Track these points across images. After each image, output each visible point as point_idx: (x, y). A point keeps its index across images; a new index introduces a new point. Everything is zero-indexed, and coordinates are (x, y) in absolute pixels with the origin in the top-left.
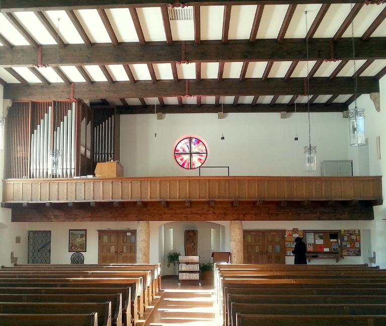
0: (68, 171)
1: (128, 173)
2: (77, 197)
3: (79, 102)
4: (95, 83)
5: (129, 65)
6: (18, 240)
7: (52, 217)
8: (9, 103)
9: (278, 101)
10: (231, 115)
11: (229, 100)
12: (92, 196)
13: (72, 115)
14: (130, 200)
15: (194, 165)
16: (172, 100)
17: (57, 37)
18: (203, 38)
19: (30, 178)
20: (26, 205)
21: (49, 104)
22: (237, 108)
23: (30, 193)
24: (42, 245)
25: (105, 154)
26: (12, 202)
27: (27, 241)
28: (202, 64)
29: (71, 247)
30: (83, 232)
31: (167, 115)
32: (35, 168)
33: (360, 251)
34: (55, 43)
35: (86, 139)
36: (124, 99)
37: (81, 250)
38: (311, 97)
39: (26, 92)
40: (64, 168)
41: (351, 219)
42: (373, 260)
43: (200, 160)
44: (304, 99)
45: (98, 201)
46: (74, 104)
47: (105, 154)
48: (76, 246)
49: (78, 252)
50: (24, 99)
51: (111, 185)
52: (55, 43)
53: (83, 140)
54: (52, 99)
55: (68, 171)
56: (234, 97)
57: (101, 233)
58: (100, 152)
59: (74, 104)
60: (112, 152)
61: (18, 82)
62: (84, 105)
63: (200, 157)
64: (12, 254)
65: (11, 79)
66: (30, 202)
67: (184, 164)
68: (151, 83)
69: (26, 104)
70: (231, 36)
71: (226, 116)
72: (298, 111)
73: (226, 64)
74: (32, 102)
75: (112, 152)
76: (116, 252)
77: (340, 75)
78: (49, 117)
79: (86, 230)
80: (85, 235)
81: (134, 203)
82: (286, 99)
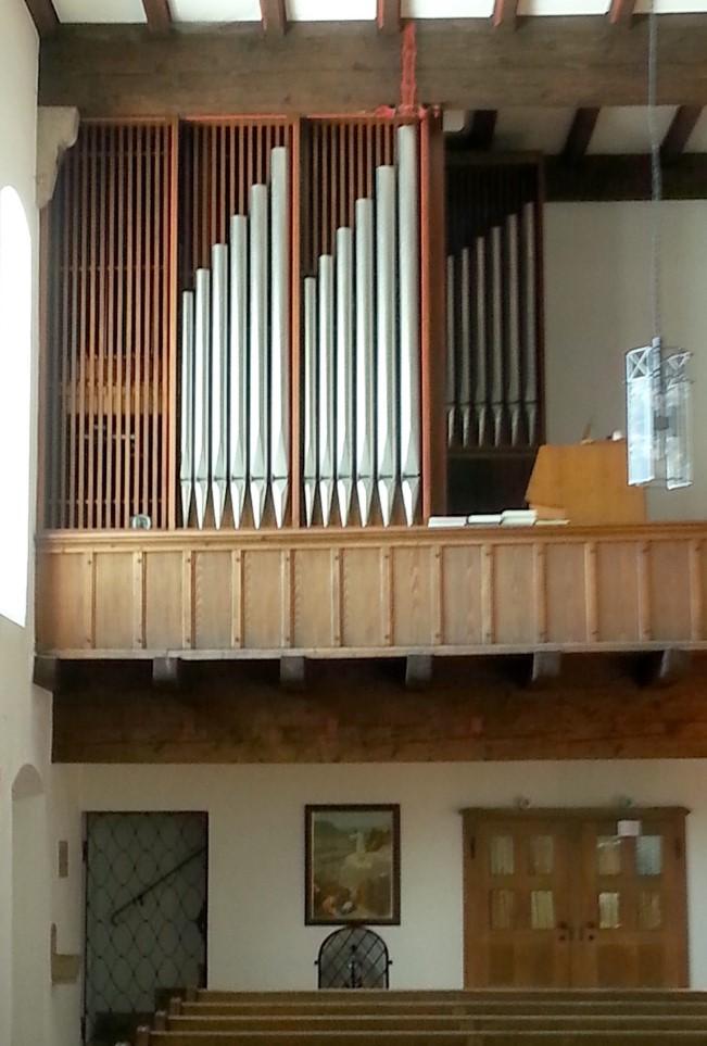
0: (257, 490)
2: (451, 631)
8: (66, 126)
14: (234, 653)
20: (169, 667)
21: (273, 135)
23: (186, 606)
24: (137, 889)
29: (319, 899)
30: (383, 820)
32: (200, 471)
37: (374, 916)
40: (275, 472)
45: (570, 646)
48: (345, 896)
49: (355, 925)
50: (151, 109)
51: (640, 560)
55: (257, 490)
57: (478, 826)
66: (188, 655)
69: (150, 136)
76: (562, 926)
79: (395, 809)
80: (389, 835)
81: (266, 671)
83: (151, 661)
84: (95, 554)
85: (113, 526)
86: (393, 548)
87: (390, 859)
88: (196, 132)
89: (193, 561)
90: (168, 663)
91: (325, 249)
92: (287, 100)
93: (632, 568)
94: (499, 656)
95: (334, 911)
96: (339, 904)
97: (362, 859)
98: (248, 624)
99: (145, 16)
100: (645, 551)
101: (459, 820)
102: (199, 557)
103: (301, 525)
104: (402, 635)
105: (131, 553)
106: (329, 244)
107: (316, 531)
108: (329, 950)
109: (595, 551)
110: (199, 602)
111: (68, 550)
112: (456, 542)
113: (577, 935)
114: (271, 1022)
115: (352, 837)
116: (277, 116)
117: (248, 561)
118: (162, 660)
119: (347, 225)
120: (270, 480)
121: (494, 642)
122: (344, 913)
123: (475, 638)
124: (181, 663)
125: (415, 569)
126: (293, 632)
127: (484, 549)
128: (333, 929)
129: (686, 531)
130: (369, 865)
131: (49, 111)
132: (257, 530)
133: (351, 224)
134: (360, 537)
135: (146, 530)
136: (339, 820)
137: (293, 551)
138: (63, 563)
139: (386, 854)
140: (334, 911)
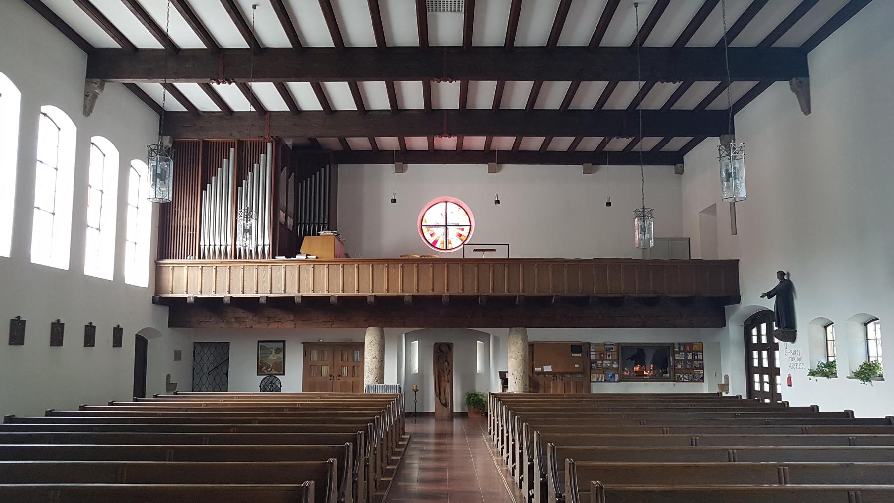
1: (368, 249)
3: (278, 142)
4: (235, 113)
5: (357, 82)
6: (178, 356)
7: (234, 320)
9: (552, 147)
10: (508, 168)
11: (505, 142)
12: (297, 288)
13: (266, 160)
15: (450, 243)
16: (419, 143)
17: (251, 38)
18: (475, 43)
19: (199, 258)
20: (192, 300)
21: (232, 145)
22: (517, 156)
25: (305, 224)
27: (192, 358)
28: (471, 83)
29: (261, 368)
31: (411, 166)
32: (207, 243)
33: (703, 378)
34: (202, 46)
35: (288, 199)
36: (315, 139)
37: (277, 373)
39: (194, 125)
40: (266, 243)
41: (691, 325)
42: (725, 387)
43: (460, 235)
44: (619, 144)
45: (305, 295)
46: (269, 144)
47: (305, 224)
50: (191, 136)
51: (326, 270)
52: (202, 46)
53: (282, 202)
54: (237, 136)
58: (308, 222)
59: (269, 144)
60: (326, 222)
61: (217, 109)
62: (285, 146)
63: (461, 232)
64: (168, 376)
65: (173, 105)
66: (199, 296)
67: (435, 242)
68: (389, 113)
70: (518, 42)
71: (500, 169)
72: (611, 163)
73: (471, 83)
74: (204, 141)
75: (326, 222)
76: (331, 376)
77: (677, 106)
78: (229, 165)
82: (591, 143)
83: (186, 298)
85: (181, 259)
86: (258, 266)
87: (282, 356)
88: (210, 143)
90: (191, 298)
91: (214, 175)
95: (265, 371)
97: (274, 356)
99: (513, 137)
101: (303, 345)
102: (204, 268)
103: (235, 259)
107: (240, 260)
108: (262, 386)
111: (165, 265)
113: (335, 378)
114: (258, 404)
116: (231, 139)
117: (217, 269)
118: (262, 297)
122: (268, 372)
123: (278, 292)
124: (196, 298)
126: (343, 288)
130: (276, 358)
133: (222, 167)
136: (267, 345)
137: (230, 266)
138: (164, 270)
139: (281, 355)
140: (265, 371)
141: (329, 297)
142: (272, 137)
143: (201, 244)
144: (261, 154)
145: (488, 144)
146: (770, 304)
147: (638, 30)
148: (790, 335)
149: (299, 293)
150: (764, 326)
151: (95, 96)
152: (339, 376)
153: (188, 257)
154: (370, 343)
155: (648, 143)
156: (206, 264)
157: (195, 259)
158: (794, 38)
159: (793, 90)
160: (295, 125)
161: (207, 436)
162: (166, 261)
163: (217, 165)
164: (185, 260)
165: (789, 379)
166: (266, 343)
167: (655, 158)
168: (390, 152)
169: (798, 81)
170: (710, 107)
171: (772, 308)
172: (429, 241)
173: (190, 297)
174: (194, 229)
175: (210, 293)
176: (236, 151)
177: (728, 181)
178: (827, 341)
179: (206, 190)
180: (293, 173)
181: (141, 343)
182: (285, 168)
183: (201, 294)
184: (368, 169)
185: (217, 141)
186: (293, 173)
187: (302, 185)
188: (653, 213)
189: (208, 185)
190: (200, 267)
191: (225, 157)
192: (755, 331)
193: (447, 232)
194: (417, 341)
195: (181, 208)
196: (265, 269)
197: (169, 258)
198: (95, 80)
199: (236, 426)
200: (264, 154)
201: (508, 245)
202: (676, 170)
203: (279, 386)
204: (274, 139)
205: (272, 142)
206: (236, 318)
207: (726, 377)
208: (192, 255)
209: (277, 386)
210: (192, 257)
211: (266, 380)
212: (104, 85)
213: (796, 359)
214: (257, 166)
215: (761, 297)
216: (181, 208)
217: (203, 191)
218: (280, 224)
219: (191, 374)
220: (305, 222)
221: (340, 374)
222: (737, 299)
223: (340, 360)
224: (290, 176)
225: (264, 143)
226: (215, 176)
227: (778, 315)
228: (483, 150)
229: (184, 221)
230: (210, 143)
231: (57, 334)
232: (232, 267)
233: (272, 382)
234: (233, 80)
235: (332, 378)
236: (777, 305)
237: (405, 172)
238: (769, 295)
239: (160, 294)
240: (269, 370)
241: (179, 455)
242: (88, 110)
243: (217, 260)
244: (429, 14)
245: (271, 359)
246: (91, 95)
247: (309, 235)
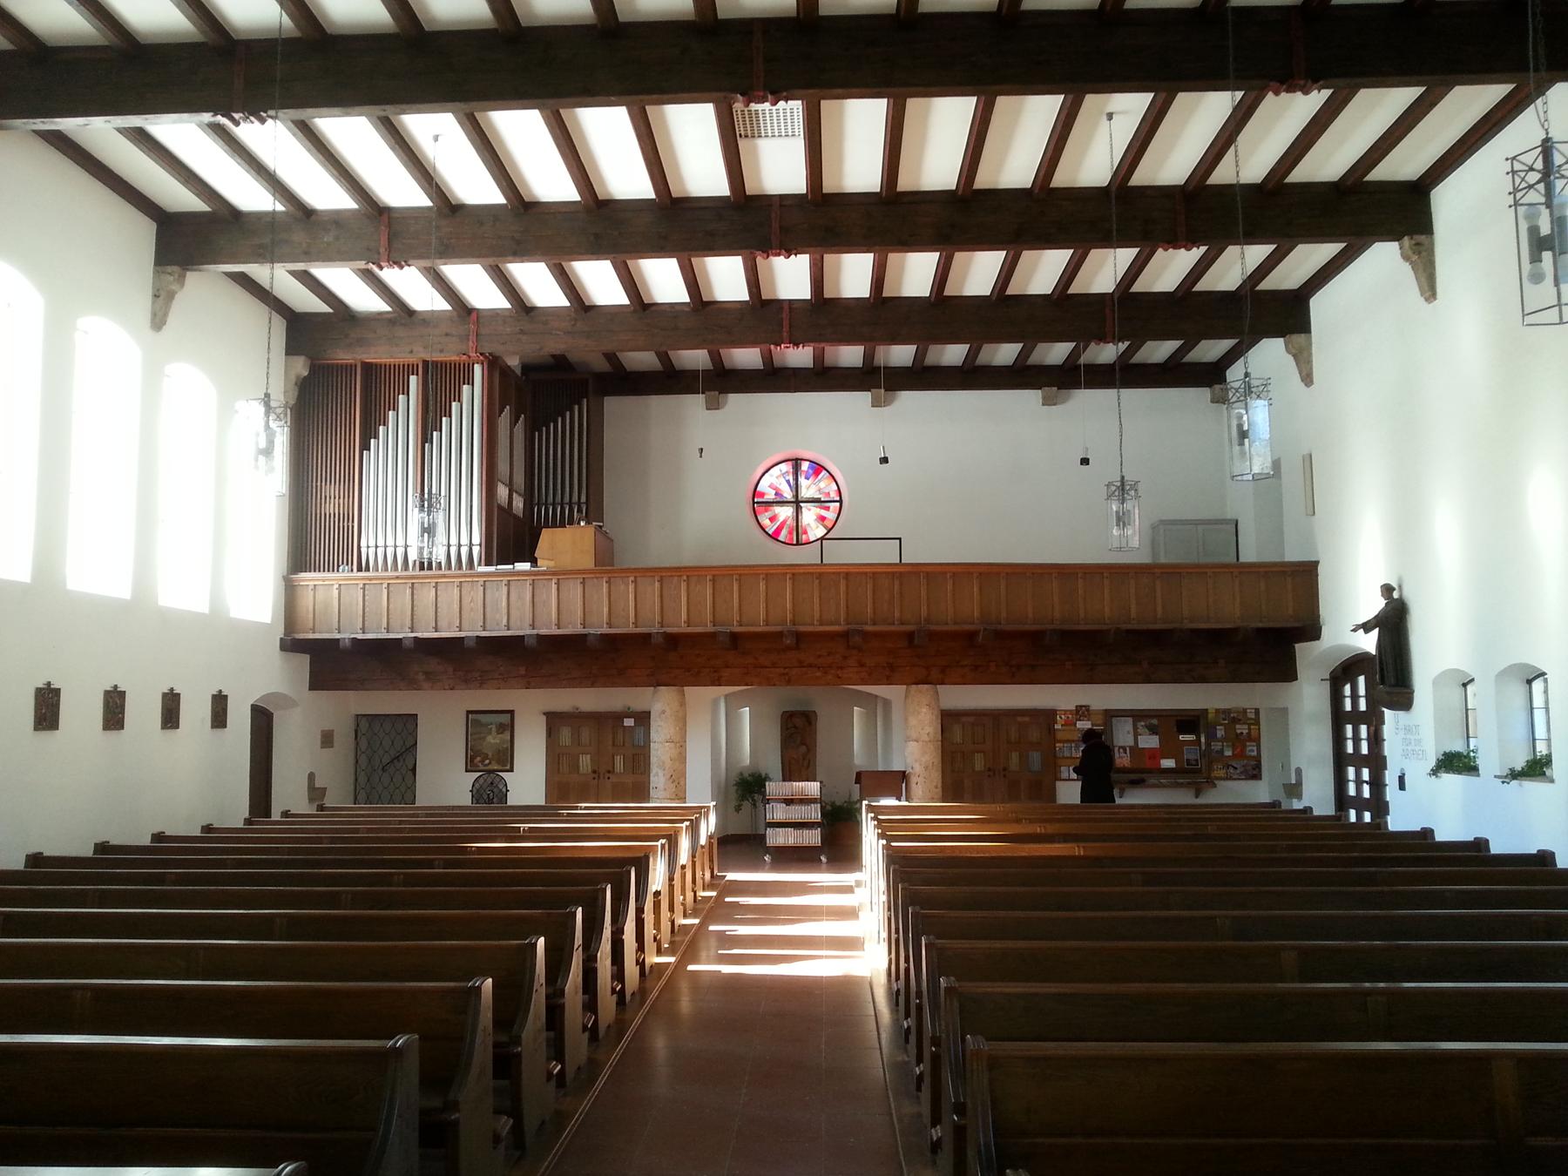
0: (390, 551)
2: (488, 622)
3: (494, 364)
4: (653, 308)
6: (327, 739)
8: (301, 367)
11: (901, 354)
12: (528, 620)
13: (473, 395)
14: (631, 629)
15: (805, 532)
16: (746, 357)
18: (829, 186)
19: (360, 569)
21: (411, 369)
22: (924, 377)
25: (538, 504)
26: (311, 636)
29: (472, 759)
30: (505, 718)
31: (733, 398)
32: (372, 543)
35: (512, 462)
37: (500, 768)
38: (1123, 346)
40: (474, 542)
42: (1295, 790)
45: (544, 632)
46: (477, 368)
48: (486, 757)
49: (493, 771)
50: (344, 356)
51: (579, 588)
53: (503, 467)
54: (420, 354)
56: (914, 347)
57: (554, 720)
59: (477, 369)
62: (506, 371)
63: (824, 513)
64: (311, 777)
65: (309, 302)
66: (360, 636)
67: (778, 531)
69: (350, 369)
75: (583, 499)
76: (594, 772)
78: (409, 405)
79: (512, 712)
82: (1056, 352)
83: (338, 639)
84: (315, 585)
85: (329, 571)
86: (461, 582)
89: (364, 589)
90: (347, 640)
92: (412, 352)
93: (652, 589)
94: (640, 634)
96: (482, 761)
98: (391, 620)
100: (581, 583)
101: (544, 718)
102: (367, 586)
104: (465, 625)
105: (333, 585)
106: (384, 422)
107: (429, 573)
108: (477, 785)
109: (558, 584)
110: (367, 609)
112: (490, 579)
113: (602, 777)
115: (489, 727)
116: (412, 359)
117: (391, 589)
119: (394, 410)
120: (386, 547)
121: (508, 629)
125: (472, 593)
127: (553, 582)
128: (481, 773)
129: (601, 573)
131: (291, 357)
132: (454, 571)
133: (395, 408)
134: (444, 576)
135: (843, 572)
137: (413, 584)
139: (507, 736)
140: (480, 764)
141: (585, 636)
142: (481, 354)
143: (362, 545)
144: (464, 384)
145: (869, 357)
146: (1368, 643)
147: (1112, 165)
148: (1403, 700)
149: (533, 629)
150: (1361, 680)
151: (171, 296)
152: (609, 772)
153: (341, 568)
154: (660, 715)
155: (1159, 351)
156: (370, 580)
157: (352, 570)
158: (1404, 164)
159: (1405, 257)
160: (522, 332)
161: (347, 892)
162: (303, 575)
163: (387, 406)
164: (335, 575)
165: (1401, 780)
166: (478, 715)
167: (1174, 374)
168: (694, 374)
169: (1413, 242)
170: (1265, 285)
171: (1372, 649)
172: (767, 530)
173: (344, 639)
174: (350, 518)
175: (449, 629)
176: (421, 381)
177: (1241, 444)
178: (1467, 710)
179: (369, 450)
180: (523, 416)
181: (262, 720)
182: (508, 407)
183: (363, 633)
184: (659, 405)
185: (388, 364)
186: (523, 416)
187: (562, 420)
188: (1140, 487)
189: (372, 441)
190: (361, 586)
191: (401, 392)
192: (1347, 689)
193: (800, 517)
194: (748, 709)
195: (321, 482)
196: (473, 586)
197: (313, 570)
198: (169, 269)
199: (402, 873)
200: (468, 384)
201: (900, 539)
202: (1213, 394)
203: (504, 790)
204: (486, 357)
205: (482, 364)
206: (426, 673)
207: (1299, 772)
208: (347, 564)
209: (501, 790)
210: (346, 568)
211: (481, 781)
212: (185, 276)
213: (1413, 742)
214: (456, 405)
215: (1352, 631)
216: (321, 482)
217: (365, 452)
218: (500, 507)
219: (353, 771)
220: (546, 501)
221: (611, 769)
222: (1312, 631)
223: (611, 743)
224: (516, 421)
225: (469, 365)
226: (384, 425)
227: (1381, 663)
228: (861, 366)
229: (328, 505)
230: (374, 367)
231: (114, 710)
232: (415, 585)
233: (492, 783)
234: (405, 262)
235: (596, 776)
236: (1380, 645)
237: (723, 407)
238: (1367, 627)
239: (294, 632)
240: (487, 762)
241: (294, 928)
242: (158, 321)
243: (390, 573)
244: (743, 144)
245: (490, 743)
246: (163, 294)
247: (554, 526)
